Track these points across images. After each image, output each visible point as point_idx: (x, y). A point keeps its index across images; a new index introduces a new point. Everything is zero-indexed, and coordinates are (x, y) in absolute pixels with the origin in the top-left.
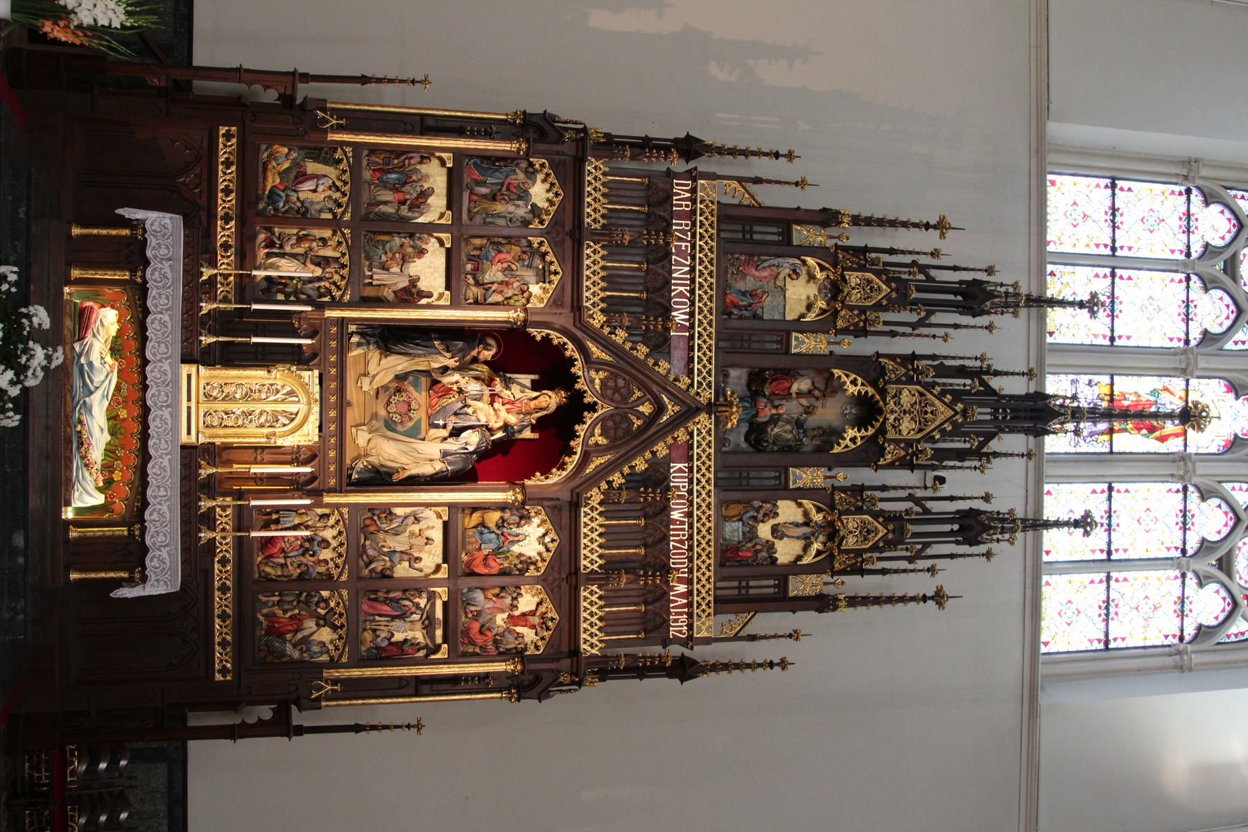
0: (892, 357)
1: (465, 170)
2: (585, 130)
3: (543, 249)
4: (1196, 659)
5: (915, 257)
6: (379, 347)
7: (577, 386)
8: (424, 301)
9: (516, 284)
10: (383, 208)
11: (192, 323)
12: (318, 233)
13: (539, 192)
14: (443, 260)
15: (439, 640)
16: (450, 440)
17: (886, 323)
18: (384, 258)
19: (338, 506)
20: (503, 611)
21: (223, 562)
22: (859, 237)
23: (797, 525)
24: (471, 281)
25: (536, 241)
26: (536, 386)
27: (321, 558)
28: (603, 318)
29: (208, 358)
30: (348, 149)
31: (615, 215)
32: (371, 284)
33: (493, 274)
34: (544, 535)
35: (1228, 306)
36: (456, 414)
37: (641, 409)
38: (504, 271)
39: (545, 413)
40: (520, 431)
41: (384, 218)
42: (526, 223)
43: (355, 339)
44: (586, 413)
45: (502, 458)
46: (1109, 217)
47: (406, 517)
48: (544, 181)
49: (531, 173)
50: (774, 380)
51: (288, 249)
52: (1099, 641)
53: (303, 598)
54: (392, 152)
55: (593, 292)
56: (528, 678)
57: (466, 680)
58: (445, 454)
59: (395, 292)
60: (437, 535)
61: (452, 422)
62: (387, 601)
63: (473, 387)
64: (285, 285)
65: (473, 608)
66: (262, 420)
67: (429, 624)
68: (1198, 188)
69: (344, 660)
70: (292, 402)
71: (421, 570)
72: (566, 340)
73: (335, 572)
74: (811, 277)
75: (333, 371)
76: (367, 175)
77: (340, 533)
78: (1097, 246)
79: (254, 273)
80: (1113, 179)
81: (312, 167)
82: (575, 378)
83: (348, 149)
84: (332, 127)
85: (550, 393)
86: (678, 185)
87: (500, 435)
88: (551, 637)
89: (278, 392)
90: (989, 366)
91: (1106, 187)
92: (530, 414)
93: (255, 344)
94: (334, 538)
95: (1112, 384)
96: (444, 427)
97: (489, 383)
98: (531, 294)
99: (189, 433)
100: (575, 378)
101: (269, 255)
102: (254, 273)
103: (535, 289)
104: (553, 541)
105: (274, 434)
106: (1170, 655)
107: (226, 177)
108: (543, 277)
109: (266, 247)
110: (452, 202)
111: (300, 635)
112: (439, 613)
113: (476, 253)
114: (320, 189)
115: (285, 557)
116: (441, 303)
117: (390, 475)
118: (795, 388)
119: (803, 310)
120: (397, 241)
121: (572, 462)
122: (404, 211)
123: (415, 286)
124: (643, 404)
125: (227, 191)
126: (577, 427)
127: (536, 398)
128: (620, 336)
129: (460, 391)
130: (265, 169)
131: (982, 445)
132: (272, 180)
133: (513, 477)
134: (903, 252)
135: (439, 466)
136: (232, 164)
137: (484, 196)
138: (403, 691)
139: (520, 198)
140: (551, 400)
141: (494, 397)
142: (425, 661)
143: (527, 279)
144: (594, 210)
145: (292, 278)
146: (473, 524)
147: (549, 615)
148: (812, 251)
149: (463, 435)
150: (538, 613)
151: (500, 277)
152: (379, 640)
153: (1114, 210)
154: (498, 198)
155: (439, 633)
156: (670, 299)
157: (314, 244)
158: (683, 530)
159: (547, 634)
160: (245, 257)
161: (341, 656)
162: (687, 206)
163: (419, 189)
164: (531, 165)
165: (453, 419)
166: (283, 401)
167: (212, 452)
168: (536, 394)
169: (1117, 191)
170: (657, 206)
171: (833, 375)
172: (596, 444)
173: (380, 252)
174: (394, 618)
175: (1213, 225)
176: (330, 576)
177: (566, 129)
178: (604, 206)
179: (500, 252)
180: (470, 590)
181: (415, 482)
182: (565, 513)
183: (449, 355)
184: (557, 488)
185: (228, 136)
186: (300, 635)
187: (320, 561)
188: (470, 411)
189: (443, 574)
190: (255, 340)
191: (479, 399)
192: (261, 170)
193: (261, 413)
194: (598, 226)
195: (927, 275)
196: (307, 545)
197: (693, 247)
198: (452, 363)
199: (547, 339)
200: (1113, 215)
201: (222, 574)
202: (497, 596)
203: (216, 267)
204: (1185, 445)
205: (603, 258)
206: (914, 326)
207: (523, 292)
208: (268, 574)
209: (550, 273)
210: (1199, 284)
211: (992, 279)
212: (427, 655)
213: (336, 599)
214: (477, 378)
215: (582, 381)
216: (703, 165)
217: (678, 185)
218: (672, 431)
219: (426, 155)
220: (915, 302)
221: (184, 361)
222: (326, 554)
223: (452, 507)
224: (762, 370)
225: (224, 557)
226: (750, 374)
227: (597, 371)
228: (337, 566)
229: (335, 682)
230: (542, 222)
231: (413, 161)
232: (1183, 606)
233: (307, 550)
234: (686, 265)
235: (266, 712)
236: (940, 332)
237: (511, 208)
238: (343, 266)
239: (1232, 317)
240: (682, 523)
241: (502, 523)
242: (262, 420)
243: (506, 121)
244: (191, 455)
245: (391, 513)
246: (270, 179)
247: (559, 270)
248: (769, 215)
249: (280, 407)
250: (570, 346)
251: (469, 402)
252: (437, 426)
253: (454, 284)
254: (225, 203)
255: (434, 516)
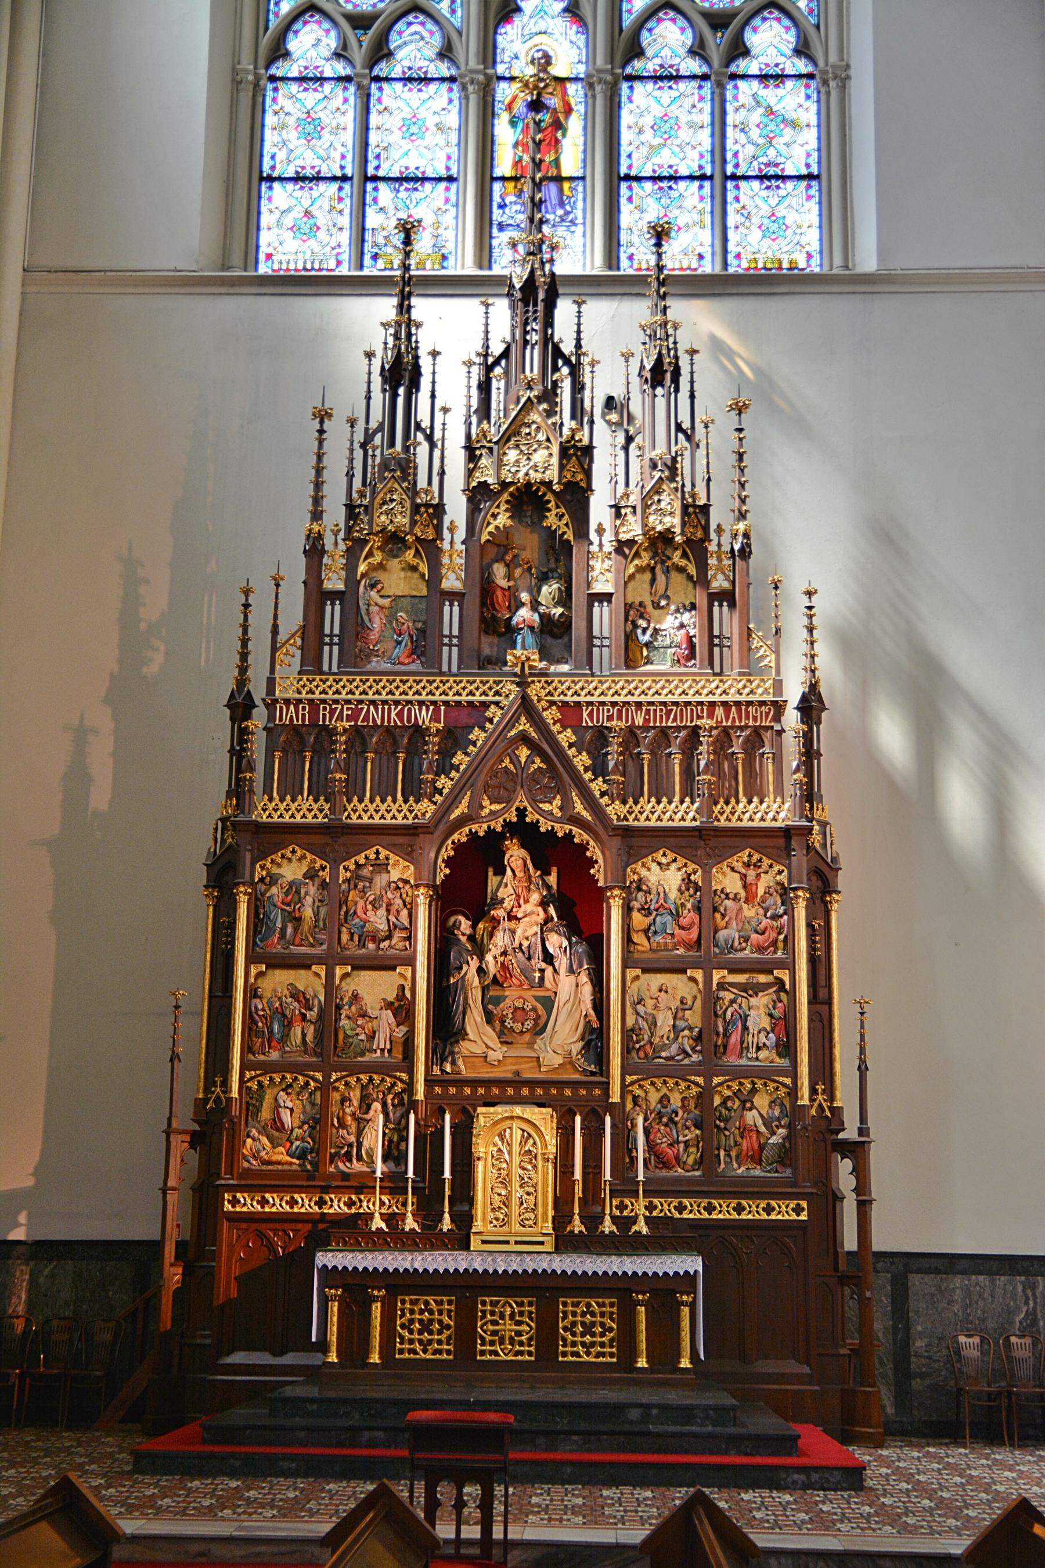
0: (470, 474)
1: (268, 950)
2: (224, 820)
3: (352, 867)
4: (833, 58)
5: (356, 446)
6: (457, 1042)
7: (499, 829)
8: (408, 994)
9: (390, 895)
10: (309, 1038)
11: (430, 1239)
12: (335, 1109)
13: (291, 871)
14: (363, 973)
15: (769, 979)
16: (557, 965)
17: (430, 483)
18: (362, 1037)
19: (624, 1086)
20: (741, 909)
21: (681, 1208)
22: (335, 514)
23: (653, 581)
24: (386, 943)
25: (343, 875)
26: (501, 871)
27: (680, 1104)
28: (425, 803)
29: (464, 1220)
30: (248, 1075)
31: (314, 786)
32: (390, 1051)
33: (378, 920)
34: (659, 864)
35: (410, 24)
36: (529, 958)
37: (523, 760)
38: (375, 908)
39: (529, 862)
40: (549, 887)
41: (319, 1036)
42: (324, 885)
43: (448, 1068)
44: (528, 820)
45: (577, 910)
46: (307, 185)
47: (638, 1014)
48: (279, 865)
49: (273, 880)
50: (494, 608)
51: (352, 1139)
52: (809, 187)
53: (722, 1125)
54: (250, 1029)
55: (394, 812)
56: (817, 883)
57: (815, 949)
58: (571, 971)
59: (398, 1025)
60: (656, 980)
61: (538, 963)
62: (727, 1036)
63: (501, 940)
64: (390, 1141)
65: (736, 943)
66: (529, 1167)
67: (752, 989)
68: (267, 67)
69: (788, 1081)
70: (511, 1135)
71: (695, 998)
72: (450, 842)
73: (694, 1090)
74: (381, 566)
75: (481, 1091)
76: (275, 1055)
77: (653, 1084)
78: (340, 199)
79: (378, 1174)
80: (262, 179)
81: (266, 1114)
82: (490, 831)
83: (248, 1075)
84: (224, 1092)
85: (507, 856)
86: (281, 719)
87: (552, 910)
88: (769, 858)
89: (500, 1150)
90: (478, 354)
91: (271, 188)
92: (530, 876)
93: (452, 1173)
94: (658, 1090)
95: (503, 179)
96: (542, 971)
97: (496, 922)
98: (400, 879)
99: (542, 1243)
100: (490, 831)
101: (359, 1158)
102: (378, 1174)
103: (395, 875)
104: (664, 855)
105: (543, 1154)
106: (828, 93)
107: (277, 1204)
108: (382, 867)
109: (350, 1161)
110: (302, 964)
111: (762, 1129)
112: (741, 978)
113: (356, 938)
114: (290, 1104)
115: (678, 1142)
116: (409, 976)
117: (593, 1030)
118: (503, 583)
119: (416, 575)
120: (344, 1022)
121: (580, 836)
122: (312, 1015)
123: (392, 1003)
124: (518, 757)
125: (292, 1203)
126: (542, 829)
127: (513, 871)
128: (444, 783)
129: (504, 953)
130: (270, 1163)
131: (567, 361)
132: (280, 1155)
133: (598, 897)
134: (351, 460)
135: (584, 978)
136: (263, 1197)
137: (296, 929)
138: (825, 1017)
139: (298, 892)
140: (515, 855)
141: (511, 917)
142: (792, 994)
143: (384, 883)
144: (306, 810)
145: (384, 1134)
146: (645, 942)
147: (746, 859)
148: (351, 567)
149: (551, 951)
150: (743, 871)
151: (382, 912)
152: (768, 1043)
153: (298, 179)
154: (297, 915)
155: (762, 978)
156: (404, 726)
157: (348, 1110)
158: (655, 711)
159: (766, 862)
160: (363, 1185)
161: (785, 1085)
162: (304, 709)
163: (289, 1000)
164: (262, 880)
165: (533, 962)
166: (510, 1145)
167: (561, 1219)
168: (508, 870)
169: (275, 174)
170: (305, 744)
171: (488, 541)
172: (561, 808)
173: (355, 1041)
174: (745, 1028)
175: (311, 45)
176: (700, 1095)
177: (223, 841)
178: (305, 801)
179: (355, 913)
180: (716, 945)
181: (600, 1004)
182: (637, 842)
183: (465, 968)
184: (607, 854)
185: (234, 1202)
186: (762, 1129)
187: (683, 1106)
188: (525, 944)
189: (699, 975)
190: (447, 1174)
191: (513, 932)
192: (270, 1167)
193: (524, 1169)
194: (327, 806)
195: (375, 432)
196: (665, 1120)
197: (348, 702)
198: (474, 963)
199: (448, 862)
200: (304, 179)
201: (694, 1211)
202: (723, 916)
203: (372, 1214)
204: (576, 79)
205: (361, 801)
206: (432, 445)
207: (398, 888)
208: (695, 1162)
209: (377, 858)
210: (383, 65)
211: (379, 353)
212: (786, 991)
213: (724, 1089)
214: (491, 935)
215: (493, 824)
216: (258, 692)
217: (281, 719)
218: (546, 726)
219: (252, 993)
220: (406, 449)
221: (467, 1247)
222: (676, 1100)
223: (625, 965)
224: (483, 620)
225: (675, 1208)
226: (487, 633)
227: (482, 807)
228: (688, 1088)
229: (813, 1091)
230: (323, 868)
231: (260, 1007)
232: (772, 76)
233: (671, 1120)
234: (368, 710)
235: (845, 1166)
236: (439, 416)
237: (309, 900)
238: (371, 1080)
239: (421, 18)
240: (648, 712)
241: (646, 911)
242: (529, 1167)
243: (215, 907)
244: (565, 1243)
245: (632, 1030)
246: (279, 1157)
247: (374, 849)
248: (312, 617)
249: (516, 1148)
250: (455, 837)
251: (516, 944)
252: (542, 979)
253: (392, 963)
254: (306, 1204)
255: (636, 983)
